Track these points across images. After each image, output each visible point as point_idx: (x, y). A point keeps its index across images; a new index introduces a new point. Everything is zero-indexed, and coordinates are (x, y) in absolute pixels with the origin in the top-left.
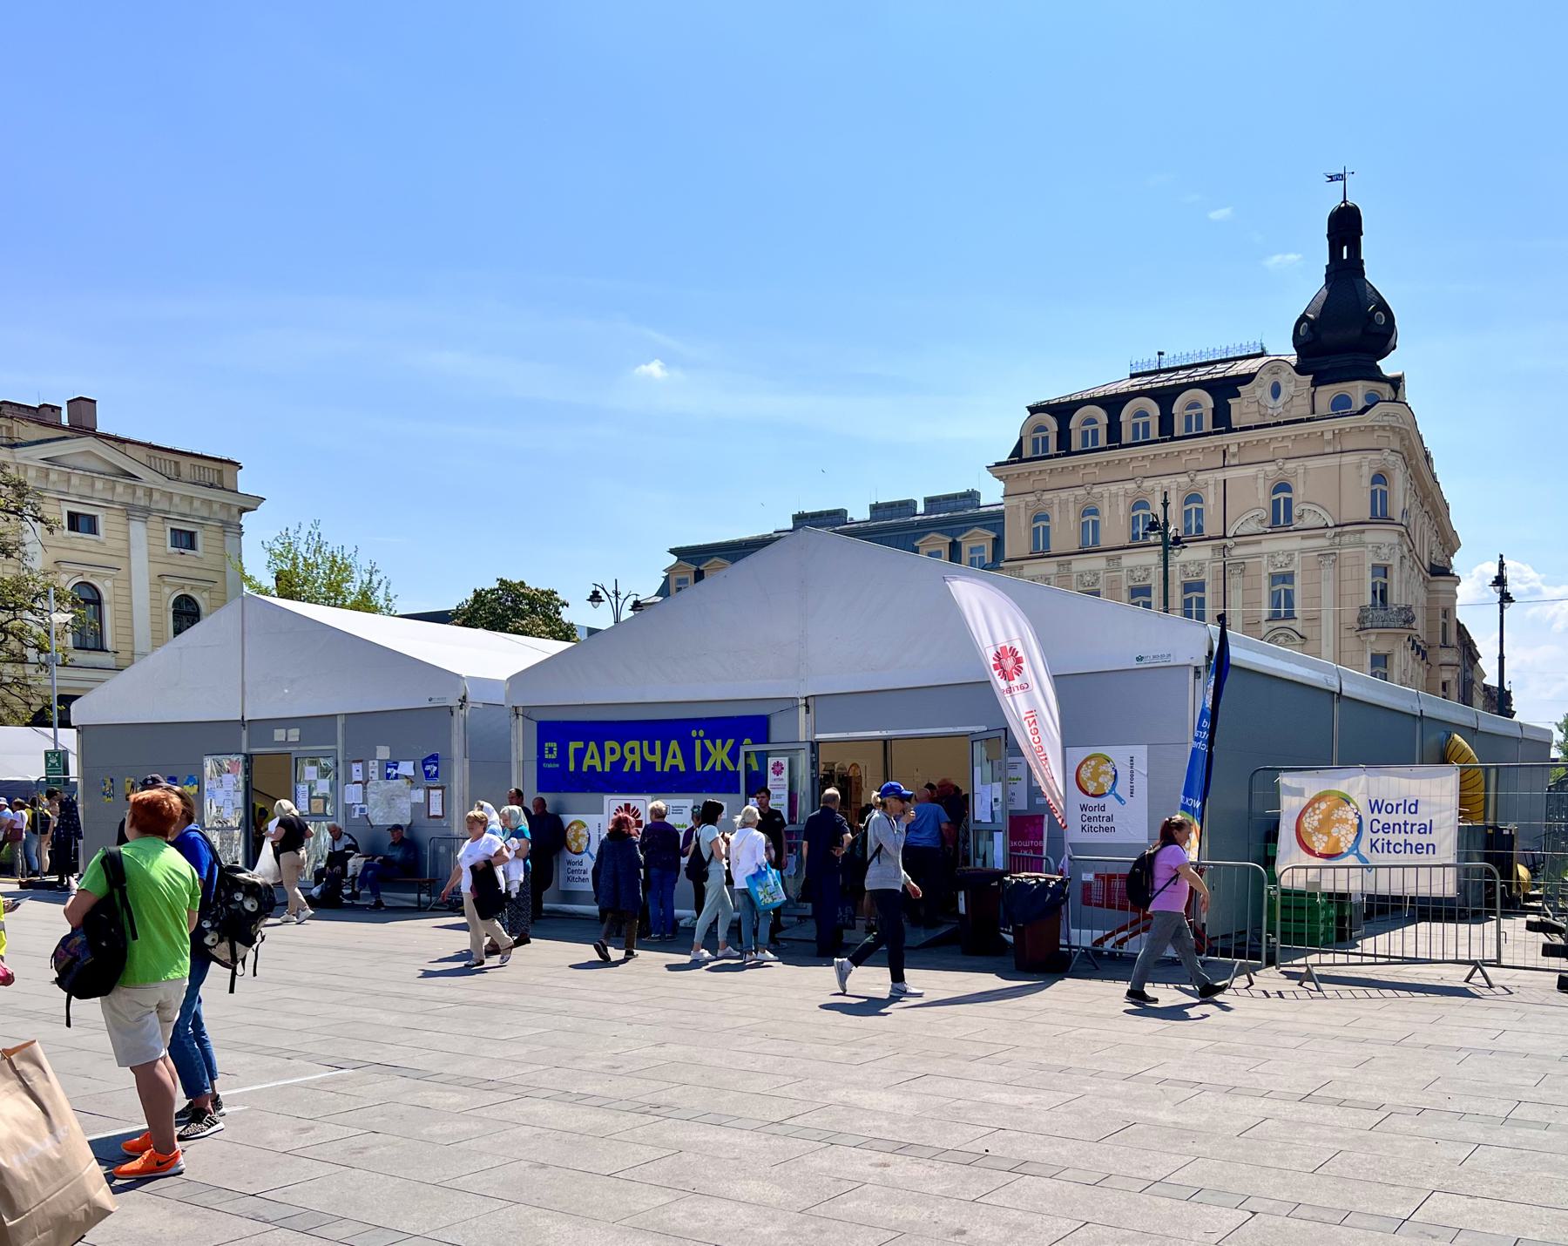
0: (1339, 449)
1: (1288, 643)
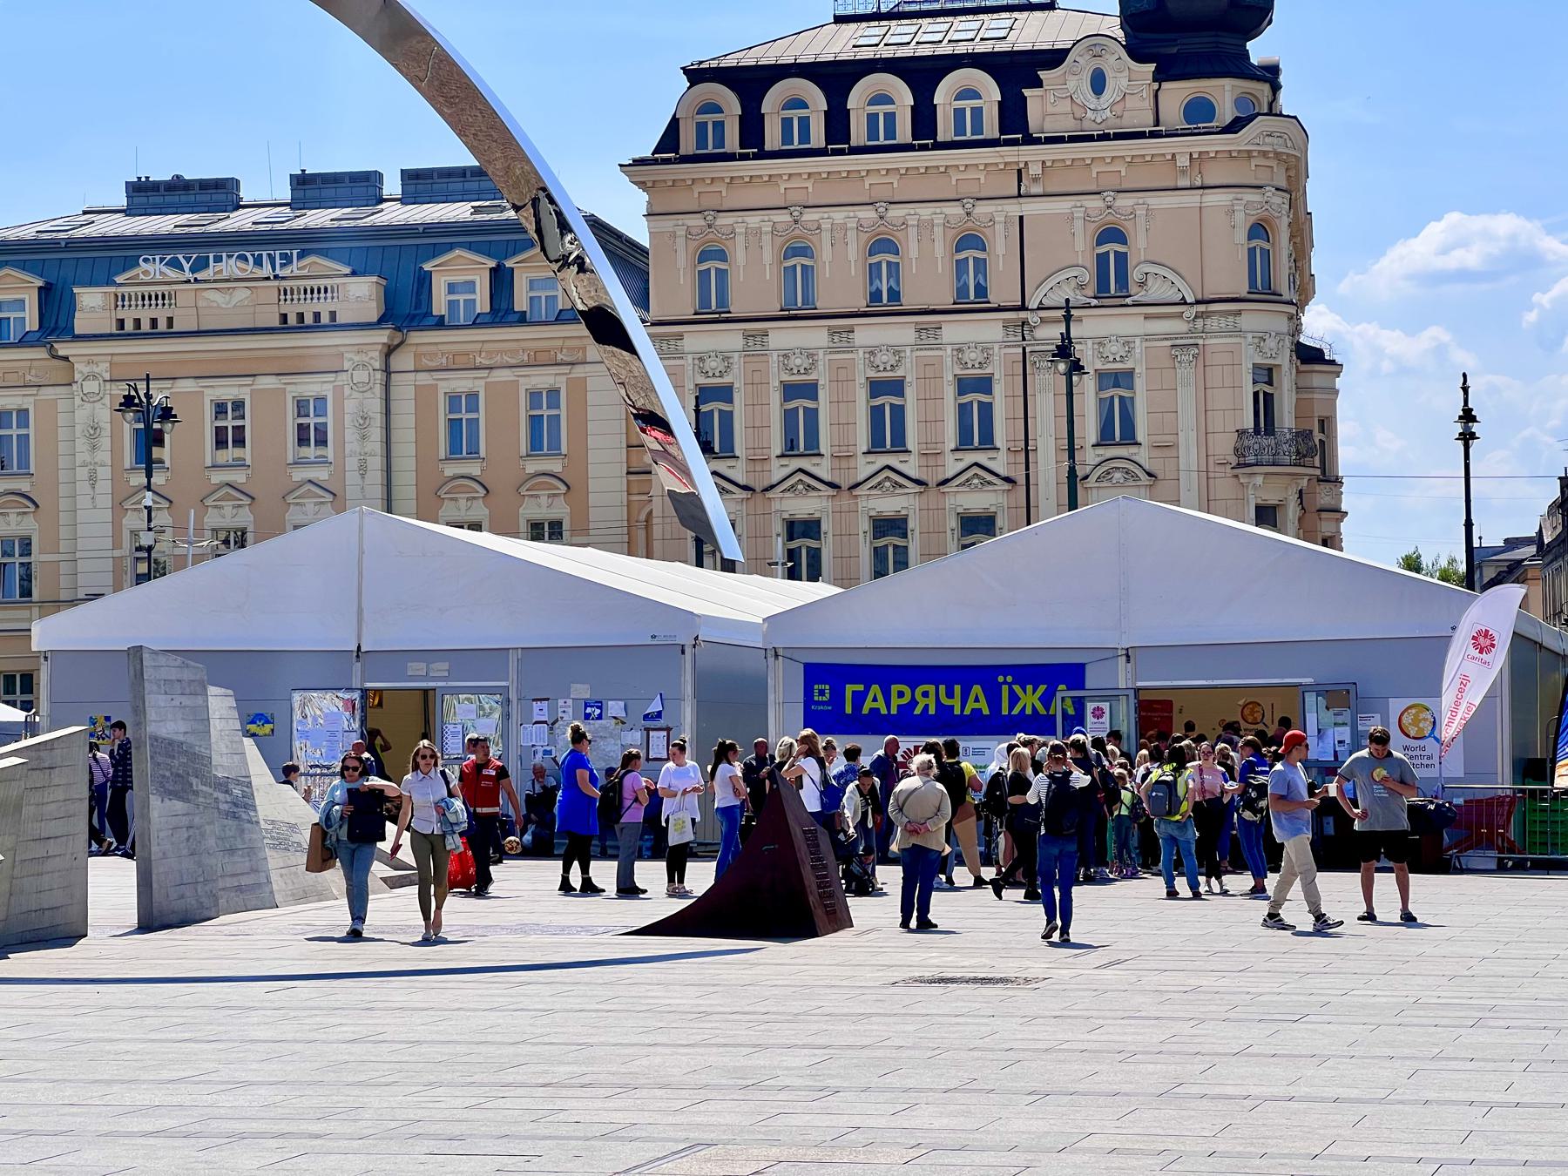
0: (1199, 183)
1: (1127, 484)
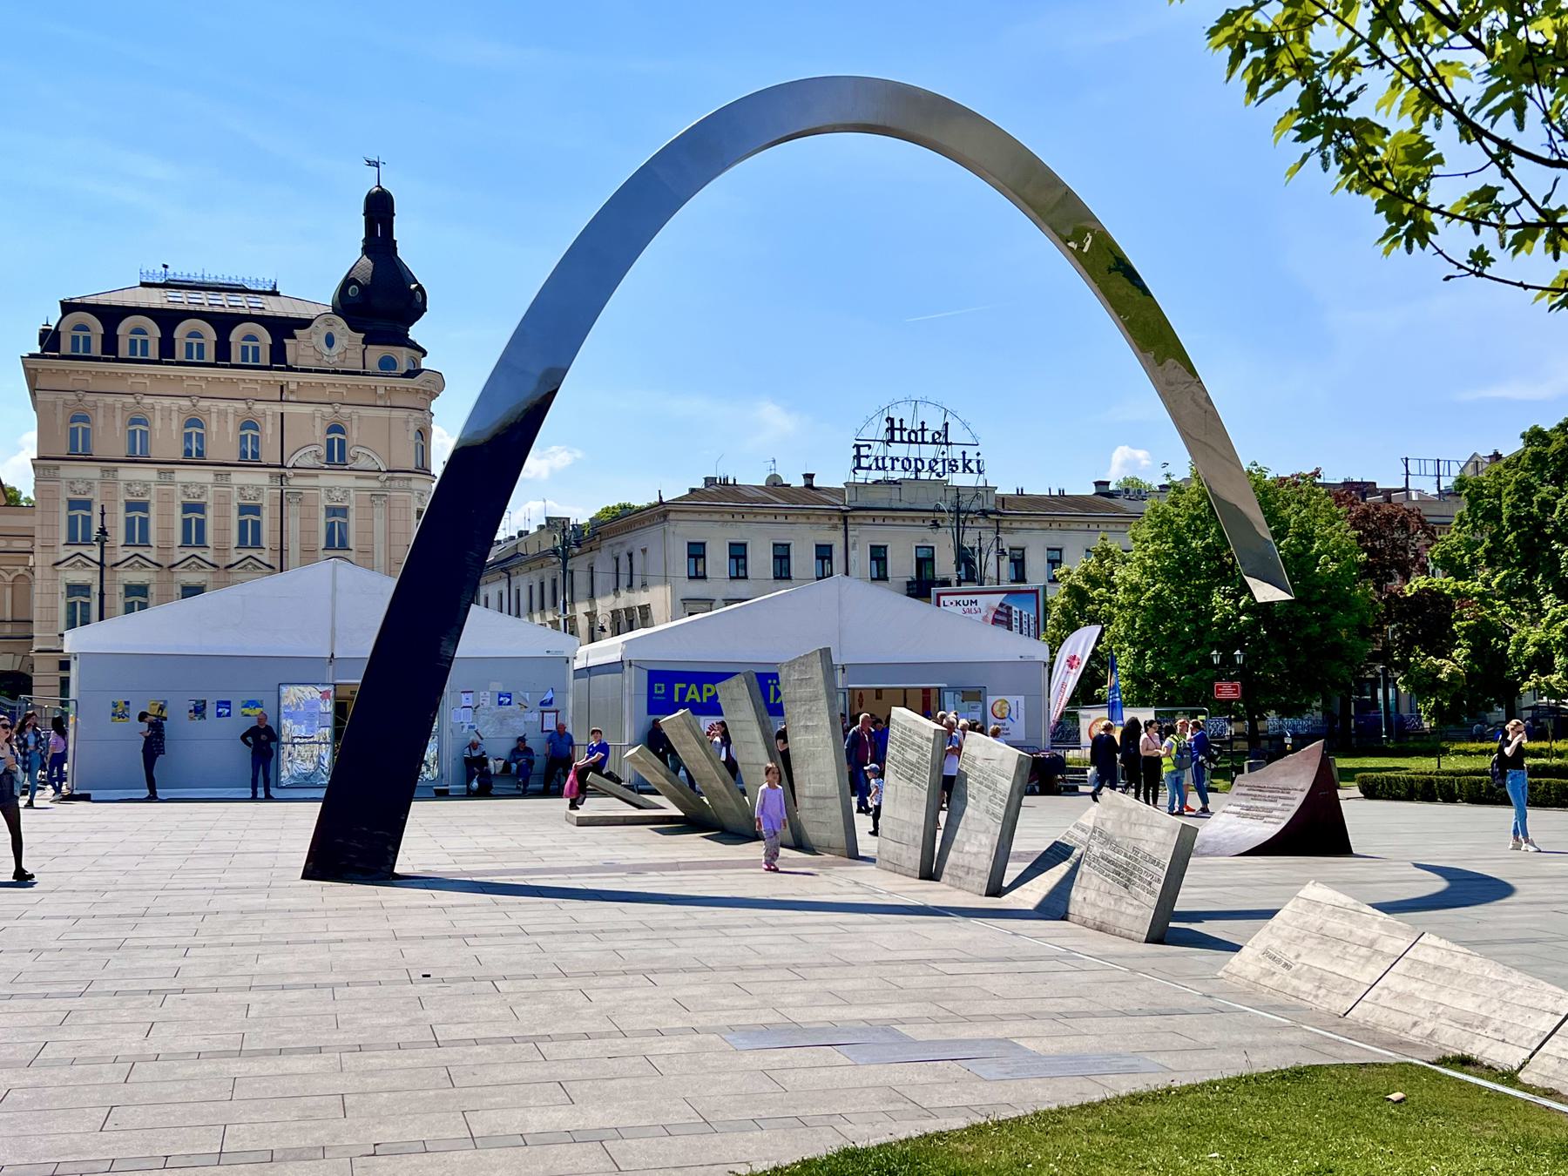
0: (389, 404)
